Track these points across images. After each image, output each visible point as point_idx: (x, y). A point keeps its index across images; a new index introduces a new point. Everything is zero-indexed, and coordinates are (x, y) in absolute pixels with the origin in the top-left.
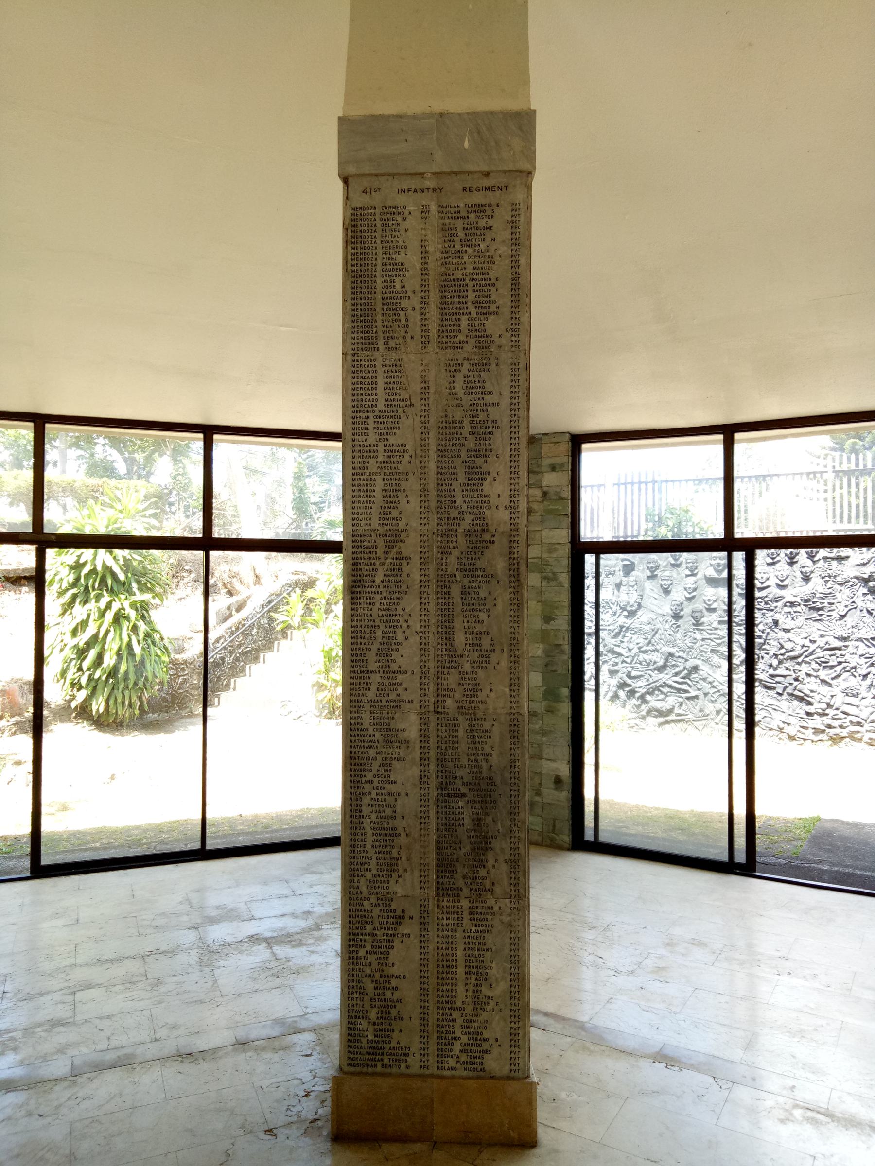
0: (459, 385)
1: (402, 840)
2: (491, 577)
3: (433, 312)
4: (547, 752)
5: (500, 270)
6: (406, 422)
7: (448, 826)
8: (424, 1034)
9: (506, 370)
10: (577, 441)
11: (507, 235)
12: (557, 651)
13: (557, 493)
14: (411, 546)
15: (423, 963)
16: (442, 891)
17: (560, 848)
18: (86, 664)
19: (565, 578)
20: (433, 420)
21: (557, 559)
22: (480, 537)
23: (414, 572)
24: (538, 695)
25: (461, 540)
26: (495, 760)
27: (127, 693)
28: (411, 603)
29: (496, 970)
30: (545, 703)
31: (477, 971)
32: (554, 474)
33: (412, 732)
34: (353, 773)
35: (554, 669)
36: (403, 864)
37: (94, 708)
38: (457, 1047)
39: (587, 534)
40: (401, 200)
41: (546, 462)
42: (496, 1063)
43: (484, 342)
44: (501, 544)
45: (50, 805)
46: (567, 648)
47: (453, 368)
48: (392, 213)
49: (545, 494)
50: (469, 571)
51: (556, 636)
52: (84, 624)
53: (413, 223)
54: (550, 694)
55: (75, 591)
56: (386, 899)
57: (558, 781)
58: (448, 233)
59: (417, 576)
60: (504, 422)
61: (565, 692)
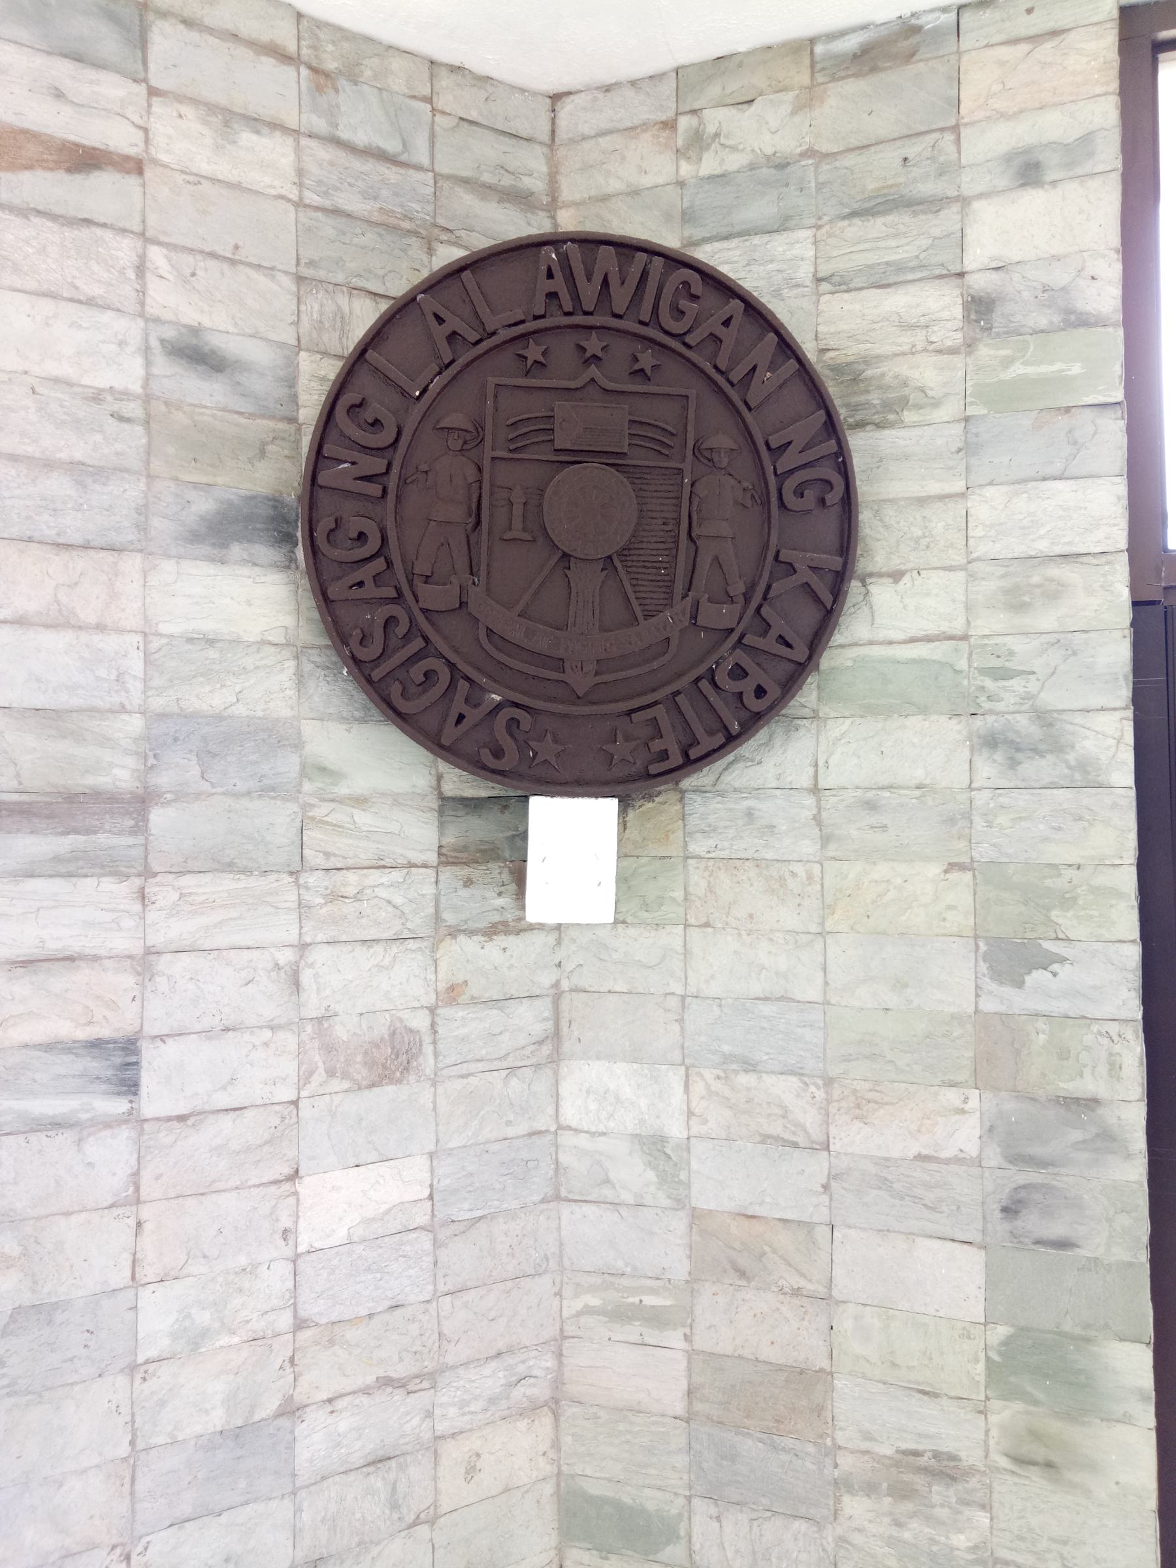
12: (1076, 1135)
13: (1050, 295)
21: (1061, 642)
24: (965, 1367)
30: (1005, 1413)
32: (1034, 200)
35: (1056, 1229)
41: (986, 143)
45: (1116, 893)
49: (980, 309)
51: (1064, 1054)
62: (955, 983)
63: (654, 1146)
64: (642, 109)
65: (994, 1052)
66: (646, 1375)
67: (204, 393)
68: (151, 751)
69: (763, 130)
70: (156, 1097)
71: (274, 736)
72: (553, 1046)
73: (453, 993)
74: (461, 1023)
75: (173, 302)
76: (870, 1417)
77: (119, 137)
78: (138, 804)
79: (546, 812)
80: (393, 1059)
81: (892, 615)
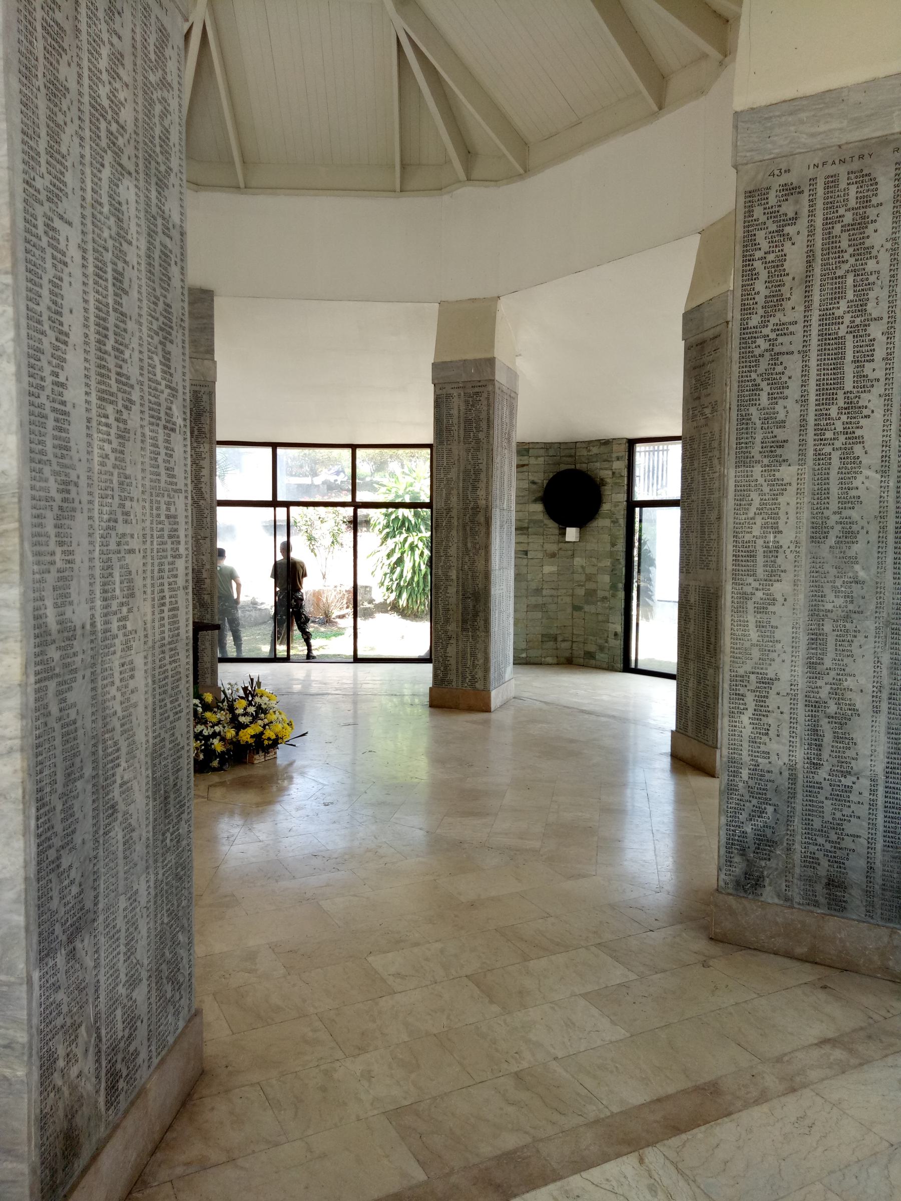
0: (470, 457)
1: (451, 612)
2: (479, 524)
3: (462, 432)
4: (611, 619)
5: (483, 415)
6: (453, 470)
7: (465, 608)
8: (457, 676)
9: (485, 451)
10: (632, 443)
11: (486, 403)
13: (620, 473)
14: (454, 513)
15: (457, 653)
16: (463, 629)
17: (616, 671)
18: (395, 577)
19: (622, 522)
20: (462, 468)
22: (476, 509)
23: (455, 522)
24: (608, 587)
25: (470, 511)
26: (480, 586)
27: (419, 596)
28: (454, 533)
29: (480, 655)
31: (474, 655)
33: (454, 577)
34: (887, 819)
36: (451, 620)
37: (401, 603)
38: (467, 680)
39: (640, 494)
40: (452, 391)
41: (614, 455)
42: (479, 686)
43: (478, 441)
44: (482, 511)
46: (623, 562)
47: (468, 451)
48: (449, 396)
49: (614, 473)
50: (472, 522)
52: (393, 551)
53: (456, 399)
54: (614, 587)
55: (387, 530)
56: (446, 632)
57: (616, 634)
58: (467, 402)
59: (456, 524)
60: (484, 469)
61: (621, 586)
62: (608, 547)
63: (582, 567)
64: (584, 445)
65: (611, 554)
66: (581, 592)
67: (534, 486)
68: (529, 523)
69: (595, 450)
70: (529, 556)
71: (542, 521)
72: (573, 556)
73: (560, 549)
74: (561, 553)
75: (531, 478)
76: (600, 594)
77: (526, 462)
78: (528, 528)
79: (568, 529)
80: (553, 555)
81: (606, 507)
